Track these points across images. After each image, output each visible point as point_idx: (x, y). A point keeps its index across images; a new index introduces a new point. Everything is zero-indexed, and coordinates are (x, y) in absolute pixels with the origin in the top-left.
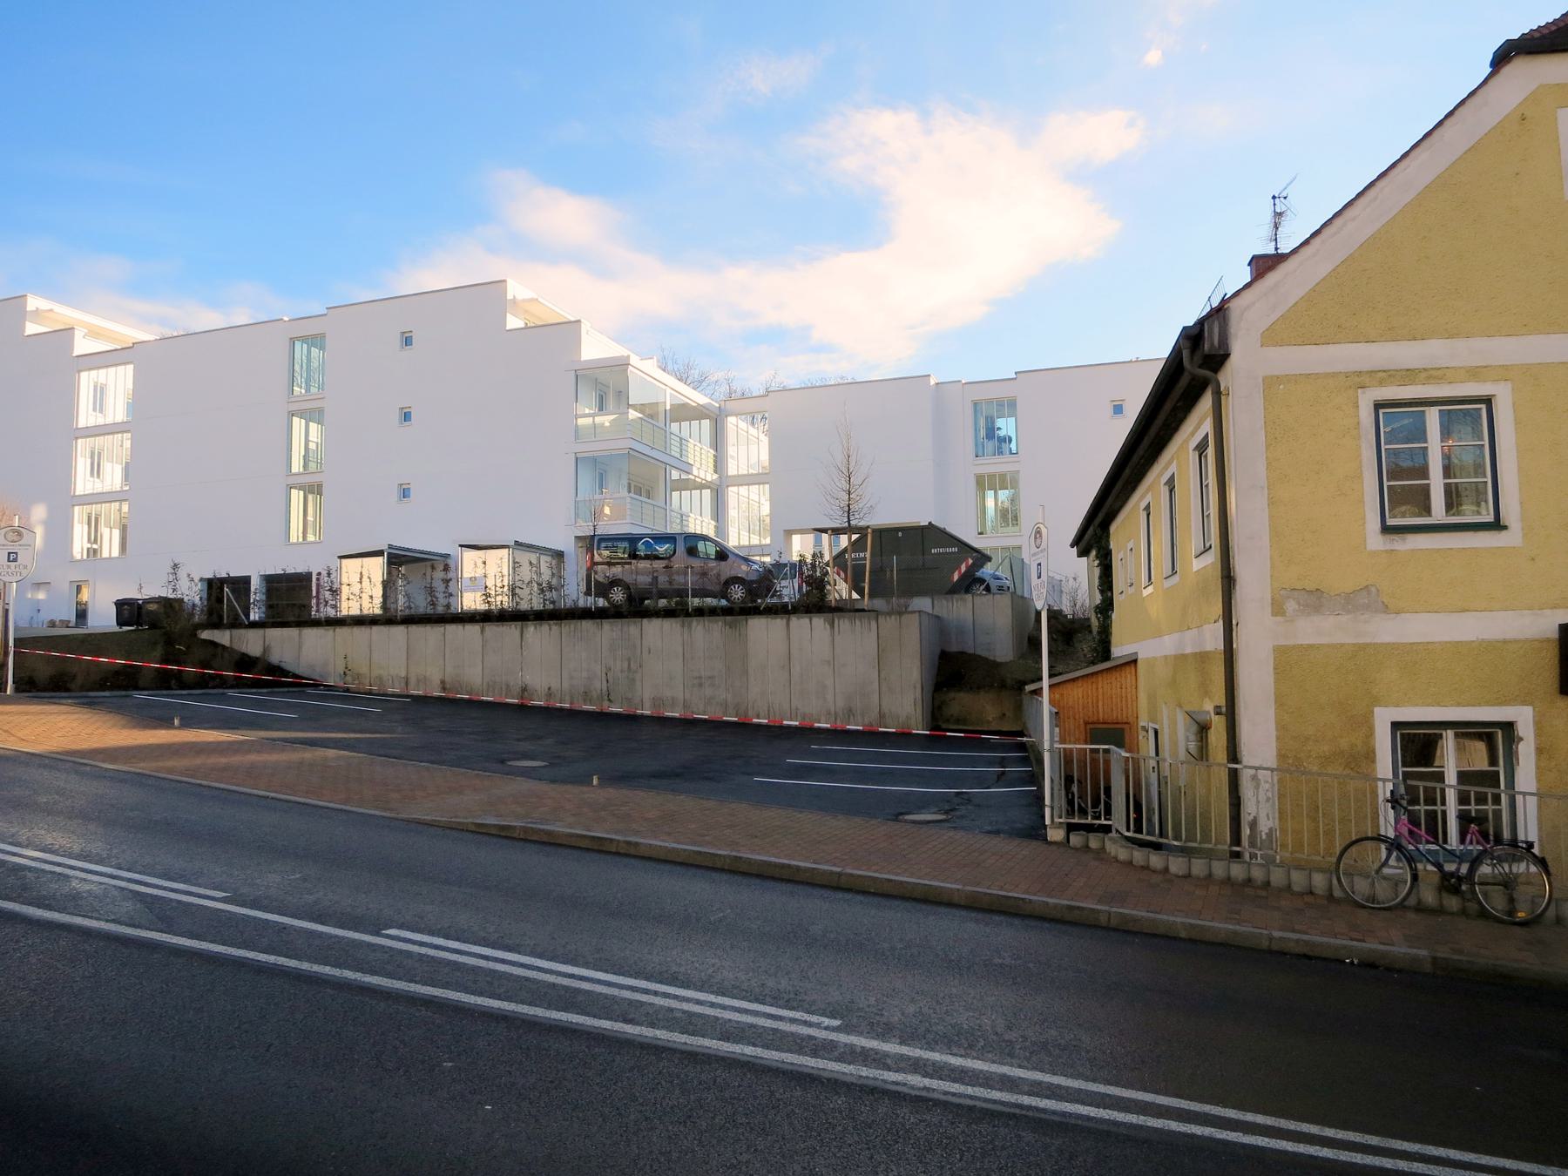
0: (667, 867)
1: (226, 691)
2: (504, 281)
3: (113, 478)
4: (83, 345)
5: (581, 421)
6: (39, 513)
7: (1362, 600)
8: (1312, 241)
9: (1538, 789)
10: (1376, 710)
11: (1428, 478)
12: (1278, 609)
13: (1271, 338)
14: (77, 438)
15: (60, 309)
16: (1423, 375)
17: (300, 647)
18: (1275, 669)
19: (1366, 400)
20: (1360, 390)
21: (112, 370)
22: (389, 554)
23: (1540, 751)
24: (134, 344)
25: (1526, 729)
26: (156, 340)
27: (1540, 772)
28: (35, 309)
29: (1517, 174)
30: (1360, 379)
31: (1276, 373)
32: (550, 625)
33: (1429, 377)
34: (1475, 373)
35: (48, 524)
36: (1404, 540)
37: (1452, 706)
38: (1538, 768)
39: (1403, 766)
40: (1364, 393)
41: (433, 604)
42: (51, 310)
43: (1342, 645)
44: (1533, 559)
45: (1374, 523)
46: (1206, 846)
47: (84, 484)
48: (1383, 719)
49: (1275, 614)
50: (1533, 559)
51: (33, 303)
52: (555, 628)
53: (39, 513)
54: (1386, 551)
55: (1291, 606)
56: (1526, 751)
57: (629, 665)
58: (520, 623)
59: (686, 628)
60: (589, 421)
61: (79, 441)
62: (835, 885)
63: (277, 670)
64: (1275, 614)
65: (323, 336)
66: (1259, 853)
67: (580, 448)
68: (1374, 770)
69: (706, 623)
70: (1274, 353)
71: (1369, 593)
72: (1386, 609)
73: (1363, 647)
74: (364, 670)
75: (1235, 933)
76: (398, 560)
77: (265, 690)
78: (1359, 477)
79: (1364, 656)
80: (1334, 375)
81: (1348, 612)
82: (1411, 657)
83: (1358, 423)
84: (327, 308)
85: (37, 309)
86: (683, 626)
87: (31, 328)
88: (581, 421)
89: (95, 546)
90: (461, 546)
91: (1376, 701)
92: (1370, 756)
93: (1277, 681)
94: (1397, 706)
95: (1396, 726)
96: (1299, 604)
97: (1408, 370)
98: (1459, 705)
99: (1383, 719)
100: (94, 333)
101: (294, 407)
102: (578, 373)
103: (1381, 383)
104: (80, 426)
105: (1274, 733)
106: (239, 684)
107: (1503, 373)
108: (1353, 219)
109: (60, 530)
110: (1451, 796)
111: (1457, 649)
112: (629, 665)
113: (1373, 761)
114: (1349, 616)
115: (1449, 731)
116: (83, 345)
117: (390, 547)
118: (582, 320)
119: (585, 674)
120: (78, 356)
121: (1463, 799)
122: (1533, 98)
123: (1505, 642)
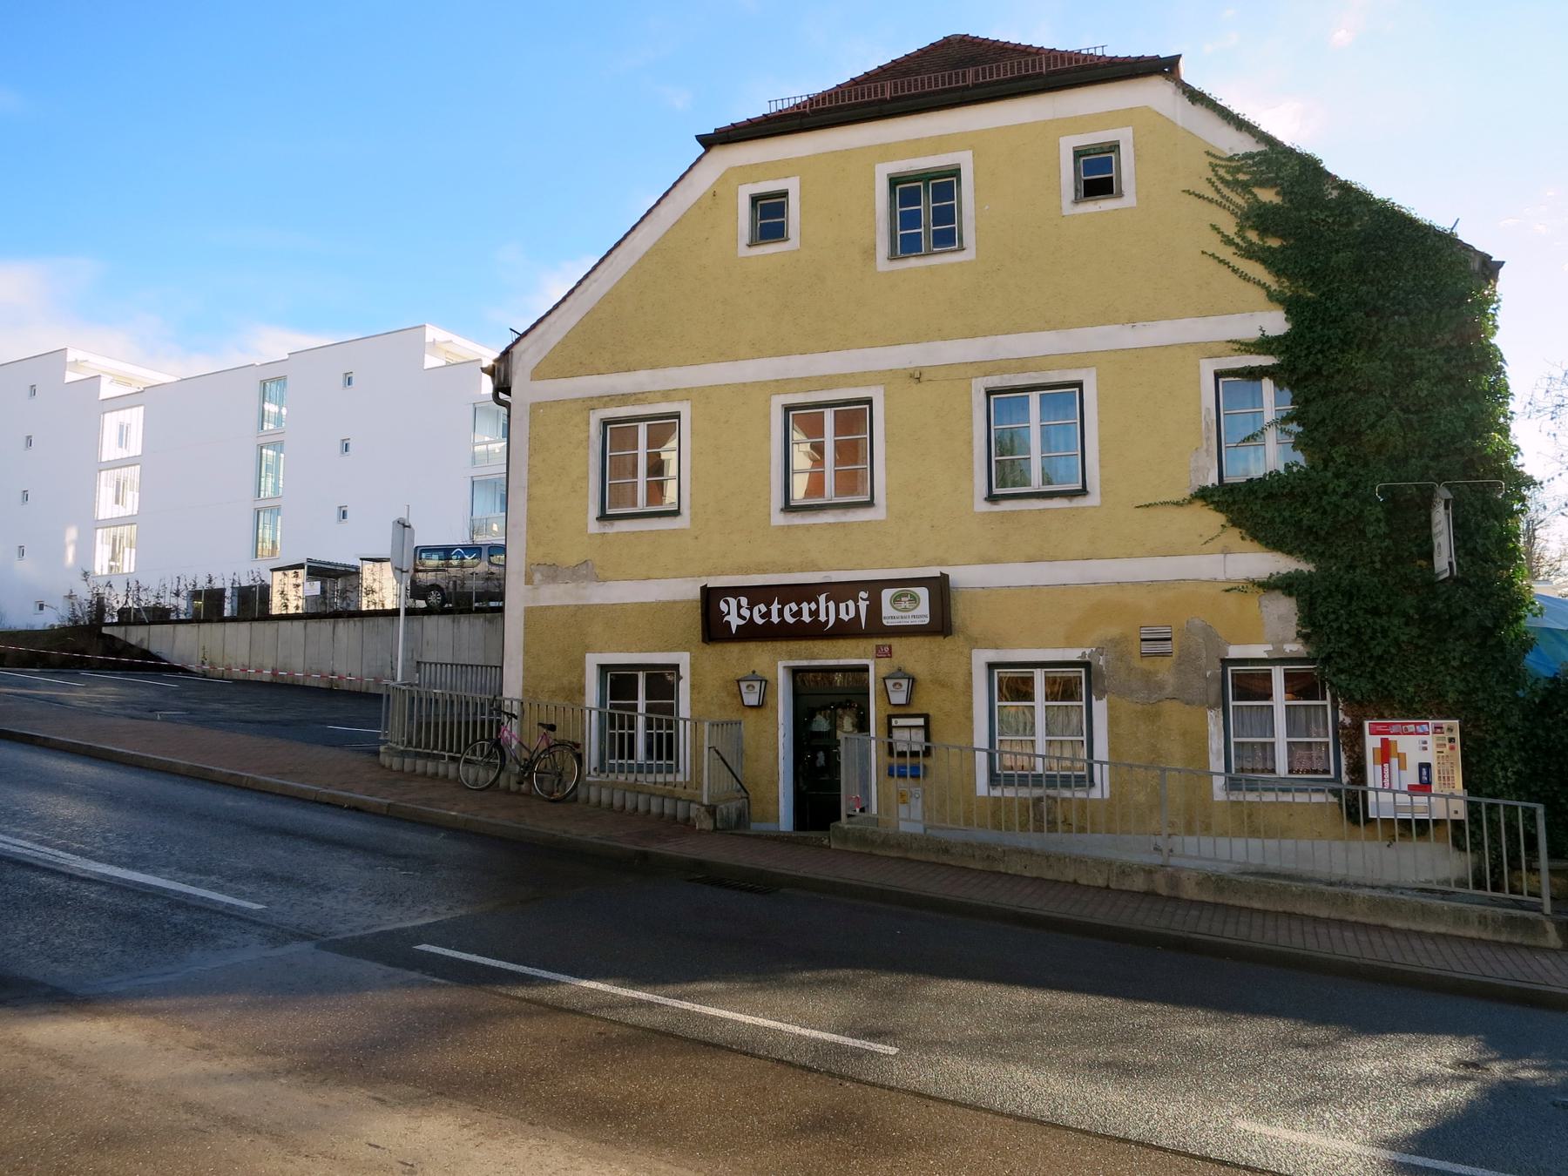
0: (270, 797)
1: (79, 671)
2: (425, 326)
3: (131, 505)
4: (107, 390)
5: (477, 449)
6: (72, 534)
7: (584, 571)
8: (568, 299)
9: (691, 716)
10: (588, 655)
11: (648, 482)
12: (529, 580)
13: (538, 374)
14: (100, 471)
15: (92, 358)
16: (633, 398)
17: (174, 642)
18: (525, 624)
19: (595, 418)
20: (591, 411)
21: (128, 411)
22: (309, 567)
23: (693, 686)
24: (145, 388)
25: (685, 671)
26: (178, 381)
27: (693, 703)
28: (74, 360)
29: (707, 239)
30: (592, 403)
31: (539, 401)
32: (355, 621)
33: (639, 400)
34: (667, 395)
35: (77, 543)
36: (612, 525)
37: (636, 652)
38: (691, 699)
39: (611, 699)
40: (593, 413)
41: (286, 606)
42: (451, 341)
43: (568, 606)
44: (696, 538)
45: (594, 511)
46: (435, 752)
47: (106, 508)
48: (593, 661)
49: (527, 583)
50: (696, 538)
51: (433, 333)
52: (358, 624)
53: (72, 534)
54: (601, 534)
55: (538, 577)
56: (684, 687)
57: (412, 655)
58: (332, 620)
59: (456, 624)
60: (484, 447)
61: (103, 473)
62: (313, 798)
63: (146, 654)
64: (527, 583)
65: (285, 378)
66: (446, 755)
67: (474, 473)
68: (584, 701)
69: (471, 620)
70: (538, 385)
71: (587, 565)
72: (597, 579)
73: (579, 608)
74: (218, 660)
75: (303, 790)
76: (318, 571)
77: (119, 673)
78: (586, 477)
79: (581, 614)
80: (576, 400)
81: (574, 581)
82: (613, 615)
83: (588, 437)
84: (289, 354)
85: (434, 340)
86: (454, 622)
87: (70, 376)
88: (477, 449)
89: (112, 563)
90: (362, 559)
91: (588, 649)
92: (581, 691)
93: (526, 634)
94: (601, 653)
95: (604, 668)
96: (542, 575)
97: (623, 395)
98: (641, 651)
99: (593, 661)
100: (119, 379)
101: (262, 441)
102: (477, 406)
103: (605, 406)
104: (103, 460)
105: (521, 674)
106: (103, 666)
107: (686, 394)
108: (595, 281)
109: (86, 549)
110: (641, 722)
111: (642, 607)
112: (412, 655)
113: (584, 695)
114: (573, 584)
115: (641, 672)
116: (107, 390)
117: (309, 560)
118: (483, 359)
119: (379, 663)
120: (103, 400)
121: (649, 725)
122: (723, 179)
123: (675, 602)
